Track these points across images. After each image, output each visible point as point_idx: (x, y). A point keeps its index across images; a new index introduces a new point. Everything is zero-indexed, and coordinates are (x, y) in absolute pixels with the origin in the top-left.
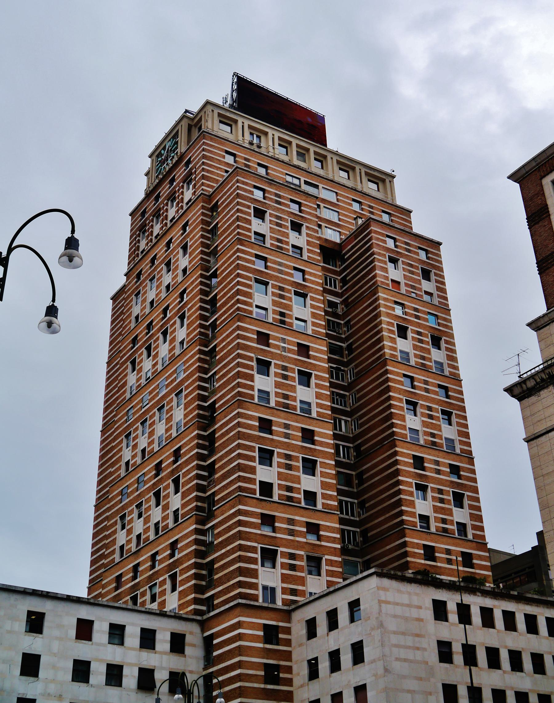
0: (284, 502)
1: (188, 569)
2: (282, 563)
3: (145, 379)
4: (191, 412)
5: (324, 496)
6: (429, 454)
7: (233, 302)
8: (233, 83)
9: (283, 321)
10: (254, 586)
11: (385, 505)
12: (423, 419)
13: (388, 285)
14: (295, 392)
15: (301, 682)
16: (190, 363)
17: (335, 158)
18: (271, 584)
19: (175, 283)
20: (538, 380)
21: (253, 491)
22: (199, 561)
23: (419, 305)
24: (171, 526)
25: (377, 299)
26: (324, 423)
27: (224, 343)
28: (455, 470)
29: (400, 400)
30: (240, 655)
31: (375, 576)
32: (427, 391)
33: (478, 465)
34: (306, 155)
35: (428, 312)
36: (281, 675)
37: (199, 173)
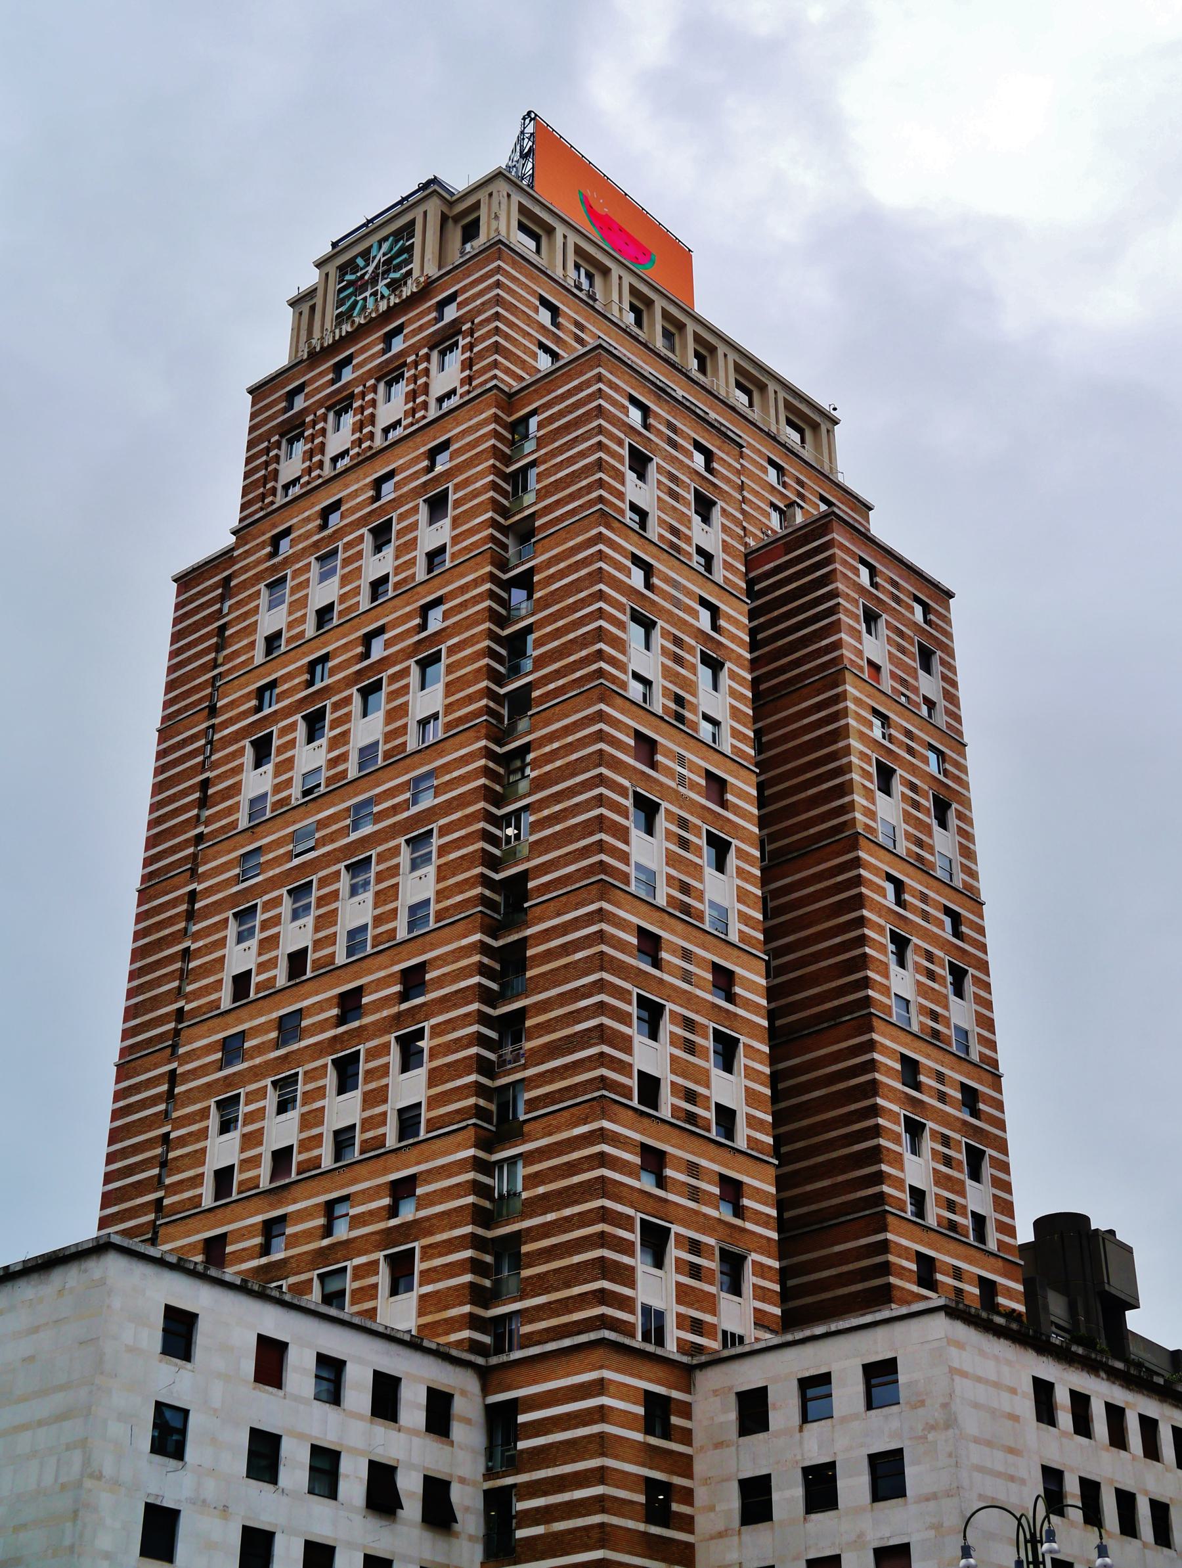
0: (683, 1125)
2: (677, 1259)
3: (300, 789)
5: (752, 1122)
6: (928, 1056)
7: (584, 653)
8: (522, 133)
9: (679, 715)
10: (626, 1303)
11: (835, 1155)
12: (919, 977)
13: (861, 669)
15: (720, 1527)
16: (455, 774)
17: (732, 356)
18: (657, 1304)
19: (405, 580)
21: (626, 1092)
22: (480, 1231)
23: (913, 725)
25: (842, 697)
26: (751, 957)
27: (556, 745)
28: (970, 1098)
29: (880, 929)
30: (603, 1455)
31: (943, 1314)
32: (925, 916)
33: (1009, 1095)
34: (677, 336)
35: (930, 744)
36: (675, 1507)
37: (484, 338)
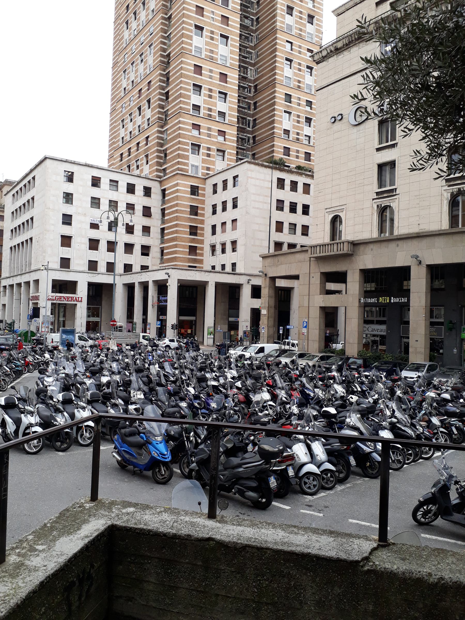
1: (153, 152)
4: (157, 58)
6: (295, 93)
10: (186, 164)
14: (218, 49)
18: (196, 164)
20: (329, 51)
24: (146, 127)
